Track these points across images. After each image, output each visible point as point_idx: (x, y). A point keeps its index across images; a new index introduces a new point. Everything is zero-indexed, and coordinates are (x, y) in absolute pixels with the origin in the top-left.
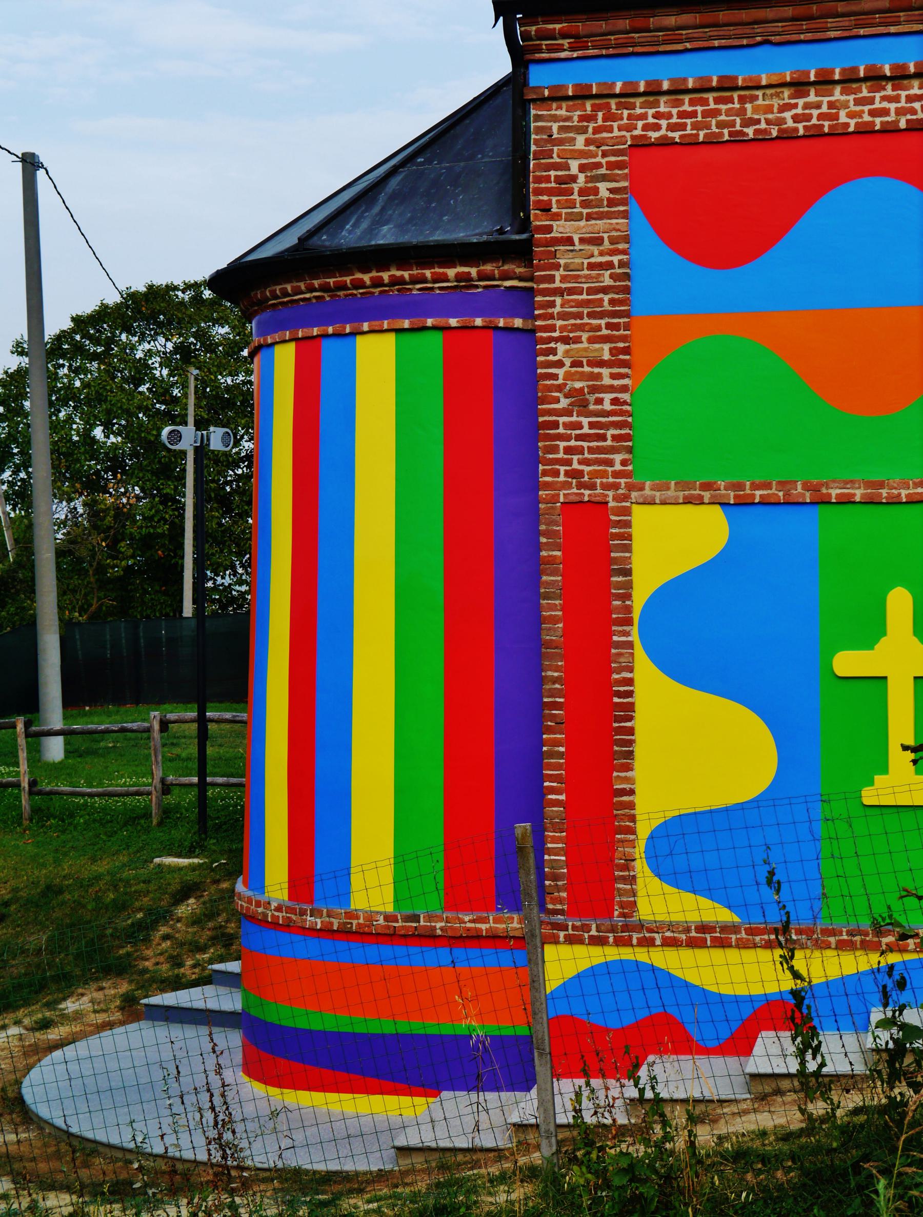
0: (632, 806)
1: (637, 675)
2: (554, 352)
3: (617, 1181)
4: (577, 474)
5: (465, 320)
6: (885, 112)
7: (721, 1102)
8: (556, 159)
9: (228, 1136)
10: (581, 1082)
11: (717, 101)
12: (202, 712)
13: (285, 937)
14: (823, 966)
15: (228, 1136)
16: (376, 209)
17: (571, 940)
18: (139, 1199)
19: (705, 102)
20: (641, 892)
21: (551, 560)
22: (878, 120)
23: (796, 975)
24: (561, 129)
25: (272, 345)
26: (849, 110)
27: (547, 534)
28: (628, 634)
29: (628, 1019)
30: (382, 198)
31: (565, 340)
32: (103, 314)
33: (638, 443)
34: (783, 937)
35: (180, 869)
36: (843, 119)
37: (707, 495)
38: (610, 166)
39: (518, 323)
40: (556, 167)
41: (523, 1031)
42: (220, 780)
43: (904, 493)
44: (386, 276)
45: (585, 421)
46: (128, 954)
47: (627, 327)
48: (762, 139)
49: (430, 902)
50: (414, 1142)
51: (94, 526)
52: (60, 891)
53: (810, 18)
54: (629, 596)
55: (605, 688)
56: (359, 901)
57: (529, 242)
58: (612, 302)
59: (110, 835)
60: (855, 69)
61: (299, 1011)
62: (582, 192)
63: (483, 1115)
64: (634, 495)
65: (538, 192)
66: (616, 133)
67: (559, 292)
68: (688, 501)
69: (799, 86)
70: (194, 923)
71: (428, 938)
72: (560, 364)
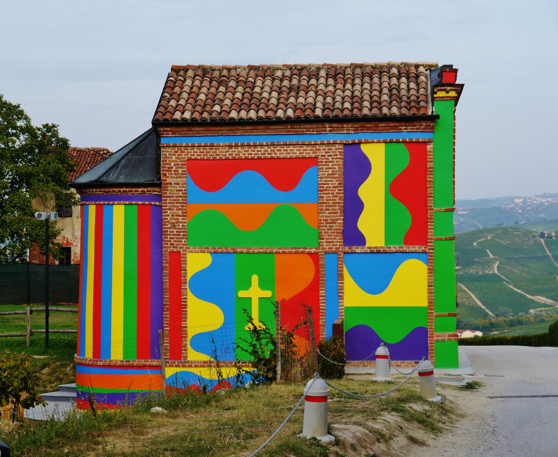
1: (188, 297)
2: (167, 212)
4: (172, 244)
5: (143, 202)
6: (251, 154)
8: (168, 162)
11: (209, 149)
12: (47, 307)
16: (119, 170)
17: (171, 366)
19: (206, 149)
21: (166, 267)
22: (250, 156)
24: (169, 154)
26: (243, 153)
27: (164, 260)
28: (186, 286)
30: (120, 166)
31: (170, 209)
36: (241, 155)
37: (206, 250)
38: (182, 165)
39: (157, 203)
40: (168, 164)
43: (256, 251)
44: (122, 190)
45: (175, 231)
47: (186, 206)
48: (220, 160)
54: (186, 276)
56: (112, 358)
58: (182, 200)
60: (244, 143)
64: (187, 250)
65: (163, 170)
66: (183, 156)
67: (168, 197)
68: (201, 252)
69: (230, 146)
70: (48, 375)
71: (132, 367)
72: (168, 216)
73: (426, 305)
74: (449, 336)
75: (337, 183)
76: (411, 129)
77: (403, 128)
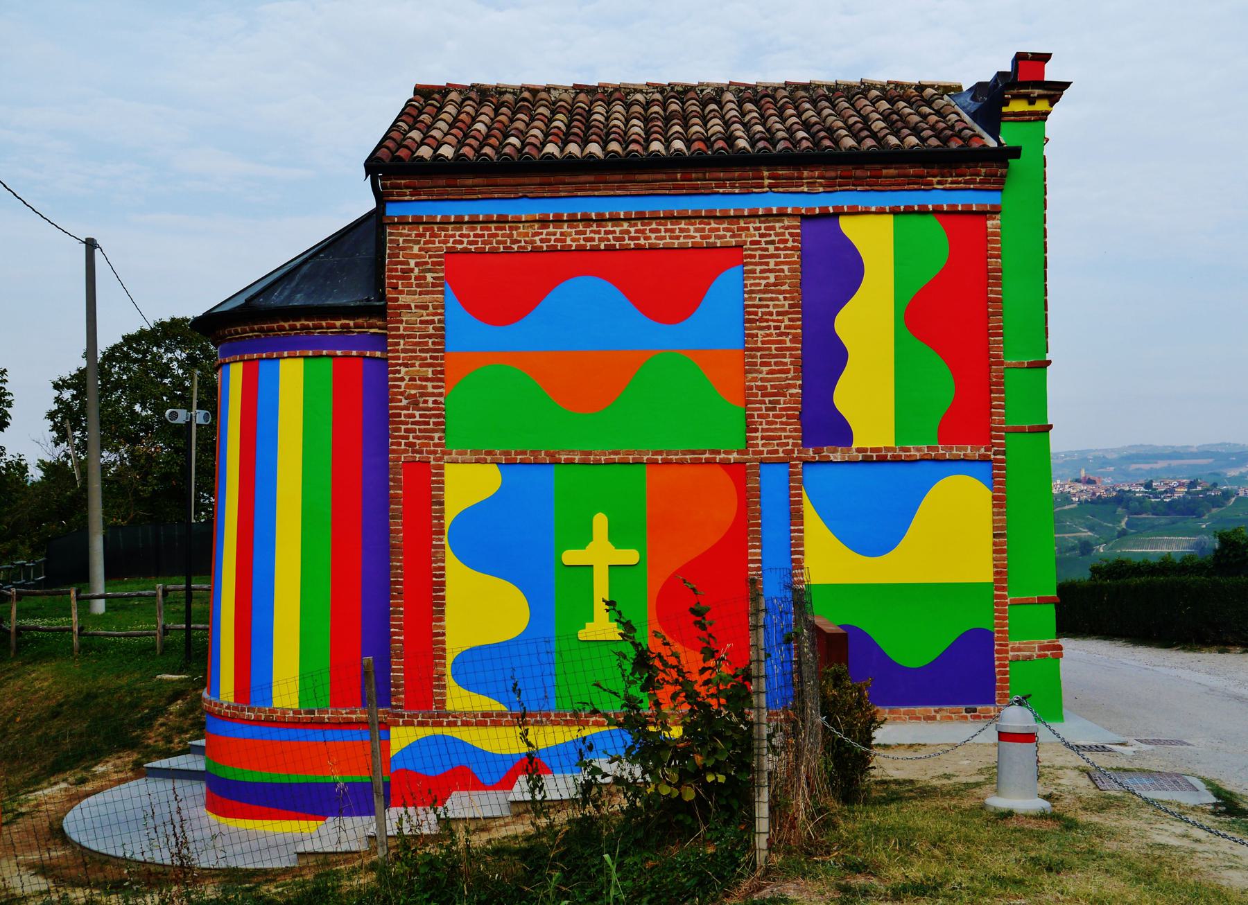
0: (443, 642)
2: (399, 372)
3: (422, 871)
5: (346, 352)
6: (592, 239)
7: (494, 818)
9: (184, 851)
10: (402, 810)
11: (496, 229)
12: (189, 583)
13: (237, 726)
14: (548, 737)
15: (184, 851)
16: (293, 284)
17: (406, 724)
18: (127, 892)
19: (490, 229)
20: (448, 696)
21: (397, 496)
23: (529, 744)
25: (229, 363)
26: (572, 237)
27: (394, 480)
29: (439, 771)
30: (297, 278)
31: (406, 365)
32: (142, 334)
33: (448, 427)
34: (522, 719)
35: (173, 682)
36: (568, 242)
37: (489, 458)
38: (434, 264)
39: (378, 354)
41: (366, 779)
42: (200, 626)
44: (298, 324)
45: (417, 413)
46: (138, 736)
48: (522, 251)
49: (322, 700)
50: (309, 849)
51: (133, 466)
52: (96, 697)
53: (550, 184)
54: (442, 518)
55: (429, 572)
56: (277, 703)
57: (385, 307)
58: (434, 343)
59: (130, 661)
60: (576, 215)
61: (238, 770)
62: (416, 278)
63: (343, 833)
65: (391, 277)
66: (437, 245)
67: (402, 337)
68: (477, 462)
69: (544, 222)
71: (320, 724)
72: (402, 379)
73: (989, 578)
74: (1042, 648)
75: (787, 303)
76: (952, 183)
77: (935, 180)
